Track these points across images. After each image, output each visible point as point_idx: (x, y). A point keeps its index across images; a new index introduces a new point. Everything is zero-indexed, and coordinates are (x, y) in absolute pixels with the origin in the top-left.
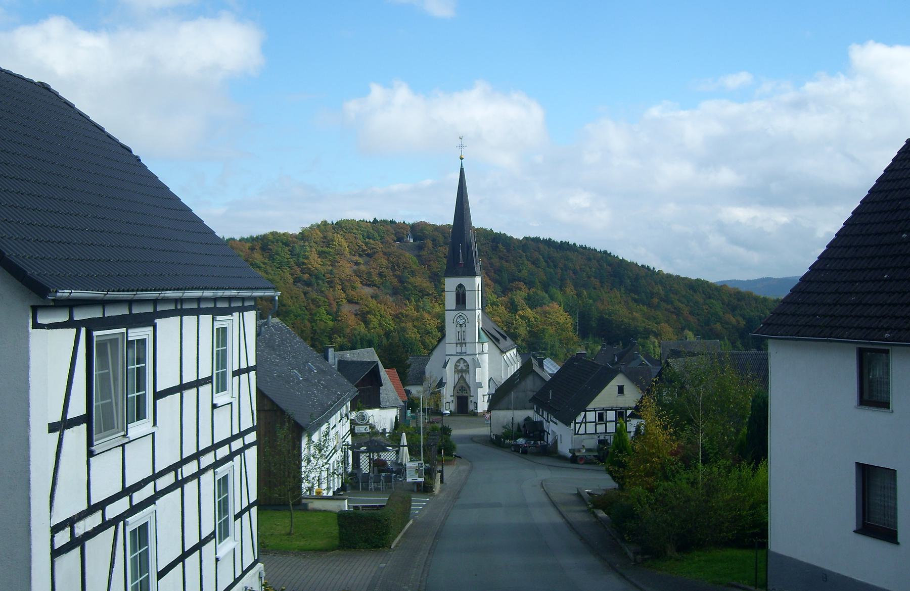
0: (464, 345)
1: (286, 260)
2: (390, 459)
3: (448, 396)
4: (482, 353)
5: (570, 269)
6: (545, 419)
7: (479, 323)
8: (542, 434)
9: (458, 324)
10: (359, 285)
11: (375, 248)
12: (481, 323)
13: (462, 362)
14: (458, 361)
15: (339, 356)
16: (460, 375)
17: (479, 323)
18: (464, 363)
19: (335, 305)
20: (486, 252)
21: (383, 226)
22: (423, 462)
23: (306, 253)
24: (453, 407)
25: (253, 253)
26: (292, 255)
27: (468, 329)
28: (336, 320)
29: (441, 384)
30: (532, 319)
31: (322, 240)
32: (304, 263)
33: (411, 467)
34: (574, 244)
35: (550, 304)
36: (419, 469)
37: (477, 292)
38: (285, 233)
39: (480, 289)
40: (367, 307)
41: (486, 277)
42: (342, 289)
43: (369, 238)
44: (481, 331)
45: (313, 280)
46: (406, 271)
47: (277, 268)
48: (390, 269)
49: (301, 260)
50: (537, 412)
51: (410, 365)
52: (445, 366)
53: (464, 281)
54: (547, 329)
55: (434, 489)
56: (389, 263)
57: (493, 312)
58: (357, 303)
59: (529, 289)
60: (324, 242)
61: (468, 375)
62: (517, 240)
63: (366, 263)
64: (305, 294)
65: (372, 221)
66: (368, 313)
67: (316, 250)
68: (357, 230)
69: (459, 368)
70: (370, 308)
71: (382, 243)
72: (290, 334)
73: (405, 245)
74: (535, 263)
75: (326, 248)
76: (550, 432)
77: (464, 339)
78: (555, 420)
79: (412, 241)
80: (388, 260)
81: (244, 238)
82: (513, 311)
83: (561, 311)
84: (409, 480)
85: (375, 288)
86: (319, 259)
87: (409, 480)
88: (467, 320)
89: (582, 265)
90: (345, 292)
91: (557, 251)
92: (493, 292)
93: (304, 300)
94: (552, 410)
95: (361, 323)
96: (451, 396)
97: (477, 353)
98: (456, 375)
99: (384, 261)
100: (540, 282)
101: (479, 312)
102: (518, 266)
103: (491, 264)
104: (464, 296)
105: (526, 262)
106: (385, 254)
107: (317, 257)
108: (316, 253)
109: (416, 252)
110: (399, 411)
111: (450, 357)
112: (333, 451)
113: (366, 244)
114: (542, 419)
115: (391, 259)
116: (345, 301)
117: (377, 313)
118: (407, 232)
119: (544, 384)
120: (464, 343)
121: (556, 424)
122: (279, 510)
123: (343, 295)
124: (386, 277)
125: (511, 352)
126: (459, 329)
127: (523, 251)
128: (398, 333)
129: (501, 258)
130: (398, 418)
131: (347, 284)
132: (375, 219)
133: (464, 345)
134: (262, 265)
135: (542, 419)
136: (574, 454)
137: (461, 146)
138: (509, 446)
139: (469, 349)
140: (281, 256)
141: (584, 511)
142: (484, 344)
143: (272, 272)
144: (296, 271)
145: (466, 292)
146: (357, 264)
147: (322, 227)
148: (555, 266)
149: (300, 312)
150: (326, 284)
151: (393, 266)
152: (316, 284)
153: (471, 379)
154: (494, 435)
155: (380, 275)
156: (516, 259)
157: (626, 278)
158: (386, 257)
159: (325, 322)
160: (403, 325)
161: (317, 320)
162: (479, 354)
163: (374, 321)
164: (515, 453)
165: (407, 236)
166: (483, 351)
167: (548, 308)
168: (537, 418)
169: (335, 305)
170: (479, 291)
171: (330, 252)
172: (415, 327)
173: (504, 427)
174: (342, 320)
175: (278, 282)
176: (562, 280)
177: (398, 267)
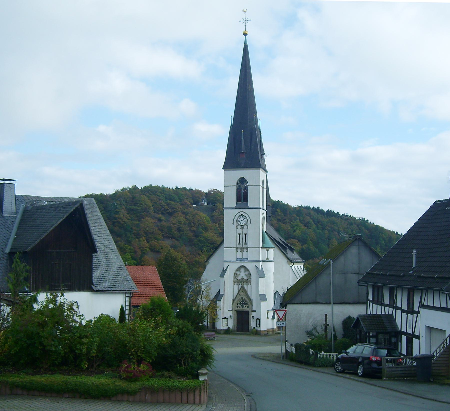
0: (245, 250)
3: (226, 310)
4: (267, 260)
5: (335, 231)
9: (239, 225)
10: (161, 237)
11: (176, 208)
13: (242, 270)
14: (239, 269)
15: (28, 202)
16: (240, 286)
17: (263, 226)
18: (245, 272)
24: (231, 324)
27: (251, 231)
29: (218, 296)
32: (116, 218)
43: (170, 200)
48: (187, 225)
52: (222, 275)
53: (246, 173)
56: (186, 220)
59: (302, 245)
61: (249, 286)
67: (126, 208)
69: (239, 278)
71: (182, 204)
74: (307, 225)
75: (134, 206)
77: (246, 243)
79: (206, 204)
80: (186, 218)
86: (128, 215)
88: (249, 220)
89: (345, 228)
90: (148, 242)
91: (325, 217)
98: (236, 286)
100: (311, 240)
102: (293, 228)
105: (300, 224)
106: (183, 213)
110: (128, 299)
111: (228, 264)
113: (168, 205)
116: (148, 250)
120: (244, 248)
124: (183, 231)
126: (239, 231)
127: (297, 215)
129: (279, 220)
130: (127, 312)
131: (150, 236)
132: (177, 187)
133: (245, 250)
137: (245, 21)
139: (251, 255)
146: (160, 220)
148: (323, 228)
150: (133, 236)
151: (190, 223)
152: (124, 235)
154: (292, 345)
155: (179, 230)
157: (382, 239)
158: (184, 215)
162: (263, 261)
166: (267, 258)
169: (139, 253)
171: (138, 209)
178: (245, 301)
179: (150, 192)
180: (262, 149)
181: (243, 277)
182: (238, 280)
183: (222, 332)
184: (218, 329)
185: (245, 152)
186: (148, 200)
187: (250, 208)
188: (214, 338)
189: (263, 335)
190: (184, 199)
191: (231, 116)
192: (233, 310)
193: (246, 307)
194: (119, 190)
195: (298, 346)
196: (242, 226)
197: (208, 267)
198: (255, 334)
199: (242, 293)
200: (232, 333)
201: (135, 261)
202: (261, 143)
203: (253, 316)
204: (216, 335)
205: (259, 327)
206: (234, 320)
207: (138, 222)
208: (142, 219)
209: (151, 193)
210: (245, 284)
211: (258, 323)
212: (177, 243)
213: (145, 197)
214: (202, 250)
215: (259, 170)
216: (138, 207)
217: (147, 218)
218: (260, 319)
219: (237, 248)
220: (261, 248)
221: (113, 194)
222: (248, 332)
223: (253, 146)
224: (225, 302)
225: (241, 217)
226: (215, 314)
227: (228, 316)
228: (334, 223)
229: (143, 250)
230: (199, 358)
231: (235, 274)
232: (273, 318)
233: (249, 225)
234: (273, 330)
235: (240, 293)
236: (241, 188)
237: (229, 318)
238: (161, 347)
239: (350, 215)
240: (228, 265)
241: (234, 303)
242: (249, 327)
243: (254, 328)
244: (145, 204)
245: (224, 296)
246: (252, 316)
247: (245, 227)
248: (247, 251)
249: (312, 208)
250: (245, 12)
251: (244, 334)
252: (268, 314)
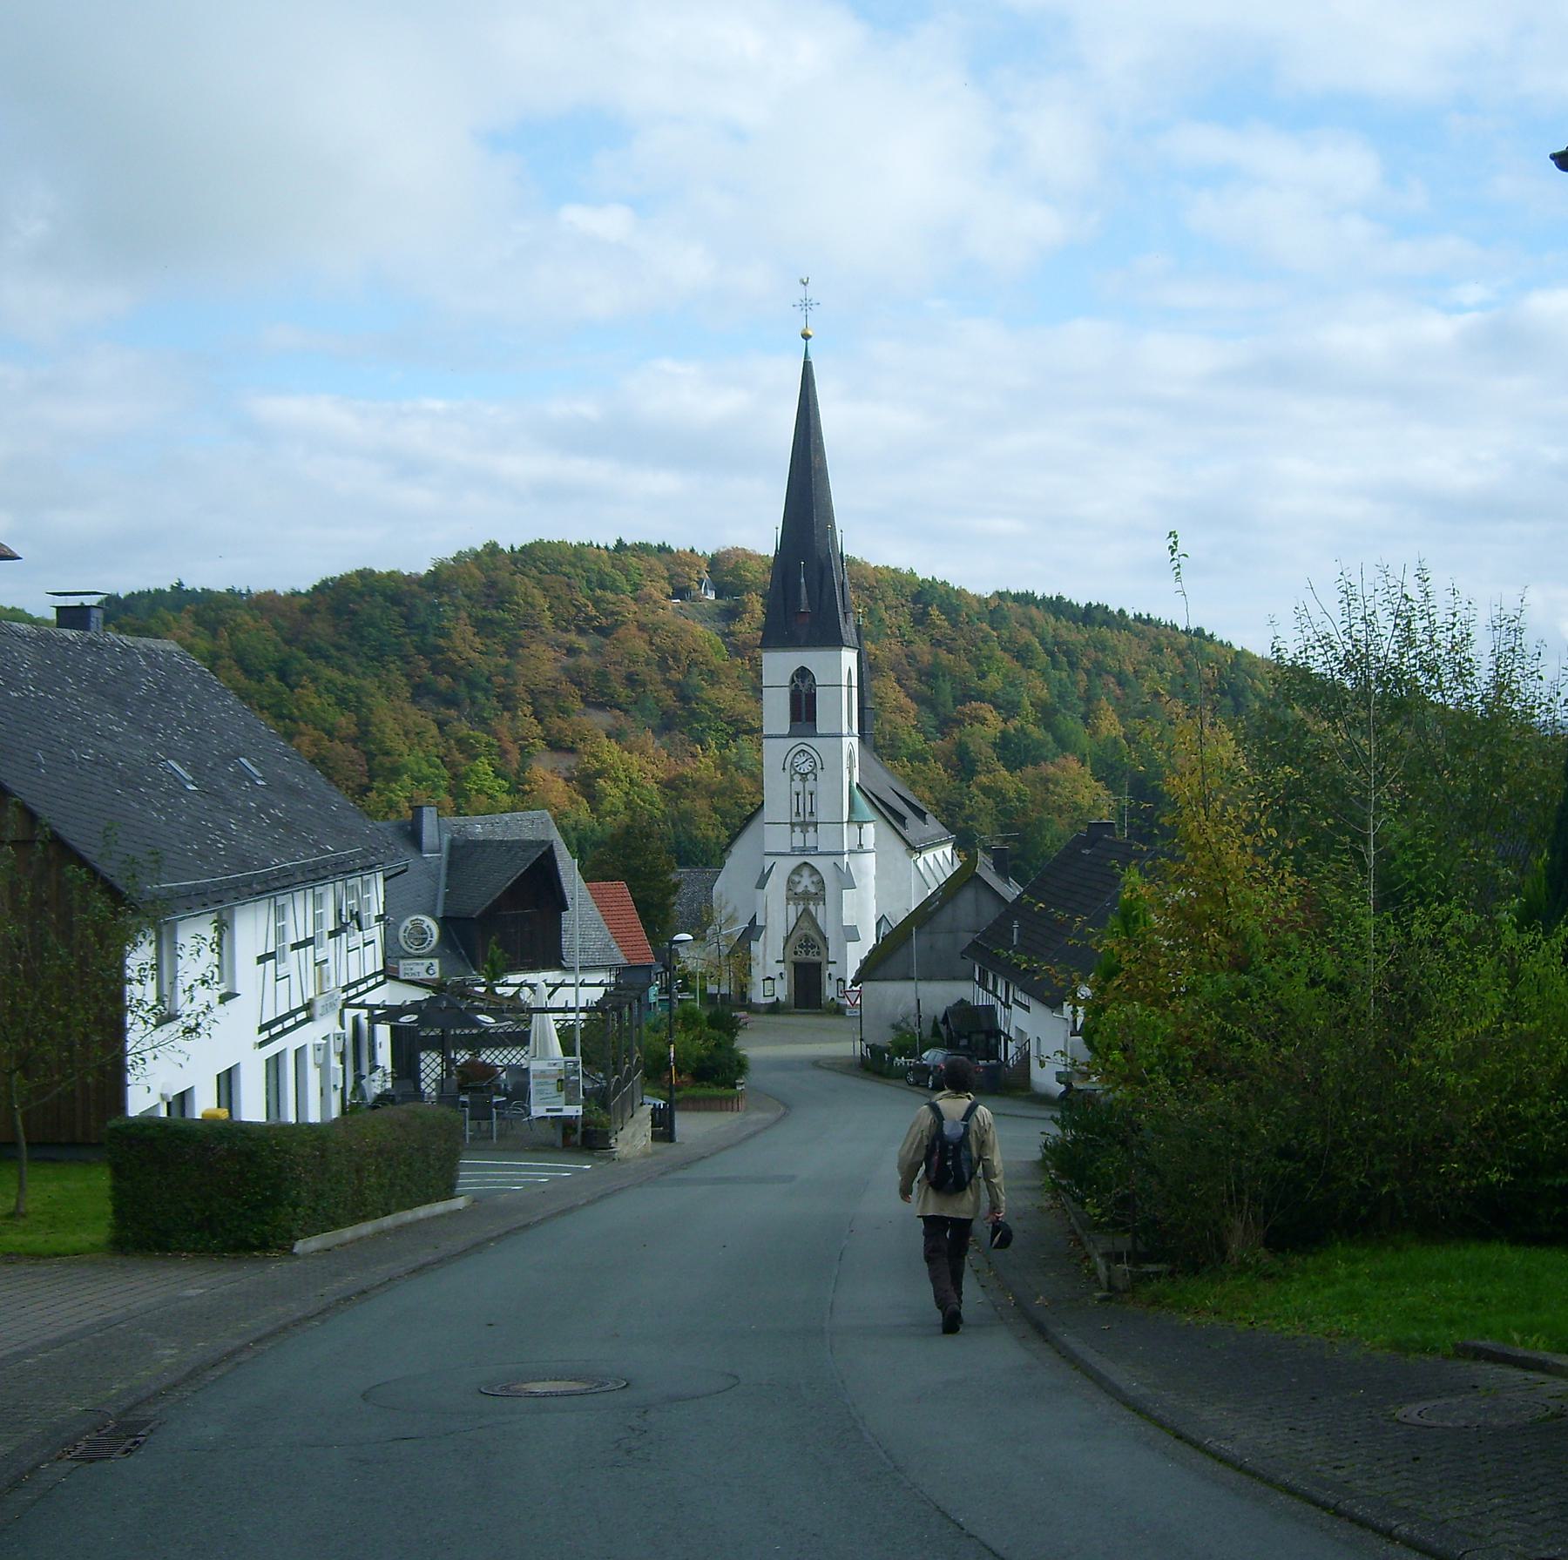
0: (811, 829)
1: (394, 640)
2: (506, 1061)
4: (860, 850)
5: (1108, 673)
6: (999, 999)
7: (851, 773)
8: (993, 1041)
9: (796, 772)
11: (618, 613)
12: (856, 771)
13: (806, 872)
14: (797, 871)
16: (801, 908)
17: (851, 773)
18: (811, 876)
19: (515, 755)
20: (899, 628)
21: (639, 558)
22: (580, 1059)
23: (445, 623)
24: (782, 991)
25: (312, 622)
26: (409, 628)
27: (823, 786)
28: (519, 791)
29: (753, 931)
30: (1012, 794)
31: (485, 590)
32: (439, 650)
33: (543, 1072)
34: (1121, 611)
35: (1057, 760)
36: (567, 1078)
37: (845, 690)
38: (393, 572)
39: (855, 682)
40: (596, 757)
41: (898, 688)
42: (536, 714)
43: (603, 587)
44: (857, 793)
45: (462, 690)
46: (695, 670)
47: (372, 659)
49: (431, 639)
50: (983, 984)
51: (677, 886)
52: (761, 884)
53: (811, 659)
54: (1049, 821)
55: (613, 1141)
56: (652, 651)
57: (914, 776)
58: (571, 750)
59: (1005, 721)
60: (489, 596)
61: (821, 906)
62: (979, 600)
63: (596, 651)
64: (441, 725)
65: (611, 547)
66: (600, 774)
67: (470, 616)
68: (574, 566)
69: (800, 889)
70: (604, 762)
71: (636, 600)
72: (206, 684)
73: (693, 606)
74: (1022, 655)
75: (494, 612)
76: (1013, 1034)
78: (1021, 997)
79: (711, 596)
81: (299, 593)
82: (963, 775)
83: (1088, 776)
84: (538, 1110)
85: (617, 712)
86: (477, 640)
87: (538, 1110)
88: (818, 762)
89: (1139, 662)
90: (540, 721)
92: (914, 727)
93: (440, 740)
94: (1016, 976)
95: (580, 798)
96: (778, 962)
97: (846, 849)
98: (792, 907)
99: (640, 645)
101: (851, 743)
103: (910, 657)
104: (812, 698)
105: (999, 653)
106: (642, 627)
107: (471, 634)
108: (468, 621)
109: (722, 625)
111: (774, 859)
112: (302, 1016)
113: (597, 602)
114: (992, 1000)
115: (657, 640)
116: (540, 743)
117: (622, 776)
118: (698, 573)
119: (1003, 910)
121: (1027, 1008)
122: (53, 1160)
123: (538, 730)
124: (644, 685)
125: (938, 852)
128: (674, 825)
129: (936, 643)
131: (547, 702)
132: (620, 541)
133: (811, 829)
134: (333, 651)
135: (992, 1000)
136: (1069, 1086)
137: (806, 305)
138: (900, 1075)
139: (823, 839)
140: (380, 630)
141: (1034, 1189)
142: (865, 825)
143: (359, 670)
144: (419, 667)
146: (572, 651)
147: (486, 559)
148: (1072, 665)
149: (426, 770)
150: (494, 701)
153: (831, 917)
154: (867, 1046)
155: (631, 680)
156: (975, 645)
158: (645, 636)
159: (491, 797)
160: (685, 804)
161: (471, 789)
162: (851, 852)
163: (613, 794)
164: (916, 1089)
165: (700, 582)
166: (861, 845)
167: (1052, 769)
168: (981, 998)
169: (515, 755)
170: (850, 686)
171: (506, 620)
172: (715, 810)
173: (895, 1027)
174: (532, 790)
175: (372, 696)
176: (1089, 698)
177: (676, 660)
187: (822, 736)
190: (643, 582)
192: (786, 960)
195: (872, 1048)
197: (730, 862)
199: (806, 924)
201: (504, 782)
203: (830, 974)
206: (789, 982)
207: (508, 661)
212: (624, 722)
214: (701, 742)
219: (792, 824)
220: (845, 825)
224: (768, 943)
226: (745, 968)
228: (1102, 646)
229: (526, 746)
230: (736, 1069)
233: (819, 773)
237: (778, 977)
238: (700, 1059)
241: (789, 944)
243: (833, 999)
246: (827, 972)
247: (811, 777)
248: (816, 831)
249: (1039, 598)
250: (805, 284)
251: (808, 1013)
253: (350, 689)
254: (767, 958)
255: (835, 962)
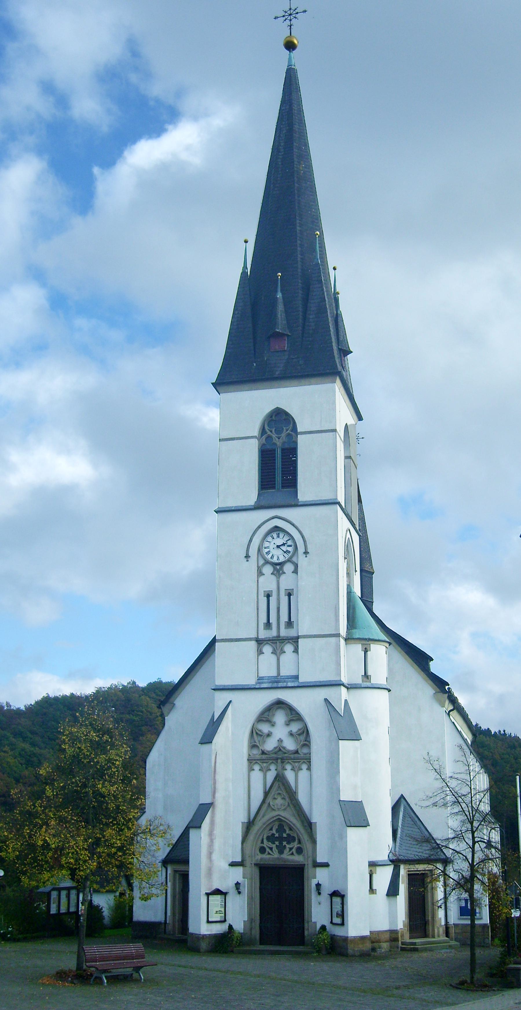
0: (289, 648)
9: (267, 562)
13: (280, 717)
16: (271, 776)
18: (288, 724)
61: (303, 774)
69: (270, 745)
77: (290, 624)
98: (257, 775)
133: (289, 648)
134: (29, 735)
145: (301, 439)
162: (350, 687)
166: (366, 676)
171: (134, 721)
178: (291, 829)
179: (157, 691)
180: (341, 334)
181: (280, 741)
182: (263, 753)
183: (204, 945)
184: (192, 934)
185: (285, 333)
186: (153, 705)
188: (137, 969)
189: (355, 956)
191: (246, 242)
192: (248, 863)
193: (294, 850)
194: (104, 688)
196: (278, 567)
198: (329, 953)
199: (279, 801)
200: (242, 948)
202: (339, 319)
204: (148, 958)
205: (343, 924)
208: (141, 738)
209: (160, 693)
210: (288, 767)
211: (337, 908)
213: (148, 699)
215: (331, 385)
216: (134, 717)
217: (149, 736)
218: (342, 893)
219: (260, 642)
220: (342, 642)
221: (93, 694)
222: (301, 945)
223: (311, 317)
224: (217, 831)
225: (275, 535)
227: (227, 885)
231: (253, 732)
232: (393, 891)
233: (302, 560)
234: (393, 936)
235: (269, 800)
236: (275, 444)
239: (511, 734)
240: (231, 701)
241: (251, 837)
242: (306, 925)
244: (148, 711)
245: (213, 813)
246: (314, 882)
247: (289, 568)
248: (296, 651)
252: (374, 875)
253: (35, 755)
254: (215, 856)
255: (326, 865)
